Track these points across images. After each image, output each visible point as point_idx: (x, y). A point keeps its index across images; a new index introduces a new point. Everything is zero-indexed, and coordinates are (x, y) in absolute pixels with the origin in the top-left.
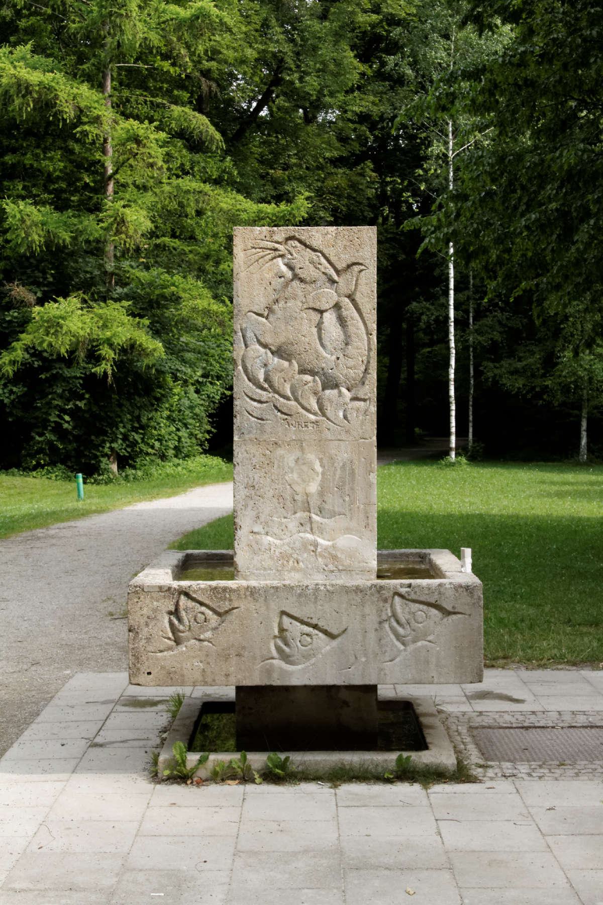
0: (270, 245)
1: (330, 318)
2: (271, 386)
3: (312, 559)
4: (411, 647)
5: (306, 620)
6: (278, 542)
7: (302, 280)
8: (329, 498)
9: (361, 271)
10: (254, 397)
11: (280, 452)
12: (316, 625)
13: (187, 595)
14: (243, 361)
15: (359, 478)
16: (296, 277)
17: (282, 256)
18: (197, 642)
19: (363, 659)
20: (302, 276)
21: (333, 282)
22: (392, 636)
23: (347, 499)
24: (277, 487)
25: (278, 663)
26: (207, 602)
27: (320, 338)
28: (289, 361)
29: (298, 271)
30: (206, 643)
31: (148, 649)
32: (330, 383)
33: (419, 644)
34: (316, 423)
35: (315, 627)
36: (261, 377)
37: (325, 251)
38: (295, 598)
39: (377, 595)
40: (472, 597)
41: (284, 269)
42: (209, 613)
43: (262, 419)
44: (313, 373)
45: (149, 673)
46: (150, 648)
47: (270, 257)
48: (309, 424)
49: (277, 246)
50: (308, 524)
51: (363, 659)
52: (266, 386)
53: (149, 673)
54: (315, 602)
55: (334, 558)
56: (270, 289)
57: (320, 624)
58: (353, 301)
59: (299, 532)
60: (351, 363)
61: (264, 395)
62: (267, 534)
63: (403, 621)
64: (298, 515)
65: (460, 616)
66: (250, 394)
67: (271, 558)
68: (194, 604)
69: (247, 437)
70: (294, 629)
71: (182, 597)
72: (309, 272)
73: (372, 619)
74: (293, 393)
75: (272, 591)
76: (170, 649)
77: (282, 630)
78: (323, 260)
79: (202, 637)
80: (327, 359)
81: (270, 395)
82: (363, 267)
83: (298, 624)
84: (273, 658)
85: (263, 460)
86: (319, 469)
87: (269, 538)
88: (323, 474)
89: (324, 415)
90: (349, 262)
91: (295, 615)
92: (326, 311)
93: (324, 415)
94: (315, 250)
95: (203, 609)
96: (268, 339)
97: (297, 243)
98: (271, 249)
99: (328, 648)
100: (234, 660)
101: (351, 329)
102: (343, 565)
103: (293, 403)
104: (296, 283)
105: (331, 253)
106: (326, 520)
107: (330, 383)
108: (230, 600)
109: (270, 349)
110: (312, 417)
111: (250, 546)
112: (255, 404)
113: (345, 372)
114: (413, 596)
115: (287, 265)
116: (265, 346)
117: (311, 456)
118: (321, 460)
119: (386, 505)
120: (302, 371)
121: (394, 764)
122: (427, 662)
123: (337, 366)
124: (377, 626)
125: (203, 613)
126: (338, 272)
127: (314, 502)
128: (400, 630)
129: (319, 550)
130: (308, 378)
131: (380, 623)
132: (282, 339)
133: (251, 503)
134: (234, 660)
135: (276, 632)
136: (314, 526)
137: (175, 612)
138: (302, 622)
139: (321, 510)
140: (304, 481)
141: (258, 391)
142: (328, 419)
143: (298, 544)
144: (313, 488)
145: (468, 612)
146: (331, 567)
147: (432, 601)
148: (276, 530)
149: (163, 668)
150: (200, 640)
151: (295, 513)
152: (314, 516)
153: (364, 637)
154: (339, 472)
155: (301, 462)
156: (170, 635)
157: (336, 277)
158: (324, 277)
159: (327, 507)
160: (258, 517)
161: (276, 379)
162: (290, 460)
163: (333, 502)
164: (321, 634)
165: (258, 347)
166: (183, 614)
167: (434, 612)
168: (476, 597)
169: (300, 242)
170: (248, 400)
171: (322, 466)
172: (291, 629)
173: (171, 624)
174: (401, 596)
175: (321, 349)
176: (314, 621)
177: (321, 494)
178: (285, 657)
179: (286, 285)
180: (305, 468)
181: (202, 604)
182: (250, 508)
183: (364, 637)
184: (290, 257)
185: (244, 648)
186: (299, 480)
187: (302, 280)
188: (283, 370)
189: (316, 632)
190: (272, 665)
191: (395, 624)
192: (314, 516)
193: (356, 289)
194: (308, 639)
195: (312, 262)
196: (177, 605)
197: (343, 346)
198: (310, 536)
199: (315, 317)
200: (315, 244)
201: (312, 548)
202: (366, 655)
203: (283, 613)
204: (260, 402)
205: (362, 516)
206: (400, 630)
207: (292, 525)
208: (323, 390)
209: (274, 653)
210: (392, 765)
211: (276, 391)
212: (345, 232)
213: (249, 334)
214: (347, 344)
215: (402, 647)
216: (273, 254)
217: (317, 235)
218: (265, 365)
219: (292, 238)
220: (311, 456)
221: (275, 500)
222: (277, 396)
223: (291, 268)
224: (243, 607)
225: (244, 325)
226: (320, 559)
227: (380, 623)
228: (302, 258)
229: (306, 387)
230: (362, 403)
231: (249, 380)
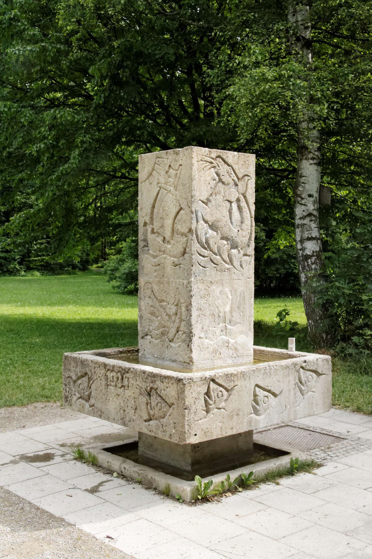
0: (210, 160)
1: (234, 206)
2: (209, 247)
3: (227, 351)
5: (266, 388)
6: (211, 342)
7: (223, 183)
8: (234, 314)
10: (201, 253)
11: (213, 287)
12: (270, 390)
13: (213, 380)
14: (196, 231)
16: (220, 180)
17: (214, 167)
18: (218, 410)
20: (223, 180)
23: (242, 314)
24: (212, 309)
26: (223, 384)
27: (231, 218)
28: (217, 231)
29: (222, 177)
30: (222, 410)
31: (195, 419)
32: (234, 246)
35: (269, 391)
37: (234, 166)
42: (223, 390)
43: (205, 267)
45: (196, 435)
46: (196, 418)
49: (212, 161)
50: (225, 330)
53: (196, 435)
55: (236, 349)
56: (209, 187)
58: (245, 197)
59: (221, 335)
61: (206, 252)
63: (304, 382)
65: (324, 376)
66: (199, 252)
67: (208, 352)
68: (217, 386)
69: (198, 278)
71: (211, 383)
72: (225, 179)
74: (218, 251)
78: (233, 172)
79: (220, 406)
80: (233, 231)
86: (230, 297)
87: (207, 341)
88: (232, 300)
89: (232, 264)
91: (262, 386)
93: (232, 264)
94: (229, 165)
95: (221, 389)
96: (208, 218)
97: (221, 160)
100: (235, 417)
101: (244, 214)
103: (218, 257)
104: (220, 184)
107: (234, 246)
108: (234, 381)
109: (209, 224)
110: (227, 266)
112: (201, 257)
114: (308, 368)
116: (206, 222)
118: (231, 291)
119: (260, 318)
120: (222, 238)
121: (289, 465)
122: (312, 403)
123: (238, 235)
125: (221, 391)
126: (238, 179)
129: (230, 345)
132: (214, 218)
133: (200, 319)
134: (235, 417)
136: (228, 331)
137: (208, 394)
138: (264, 390)
140: (224, 304)
142: (234, 267)
143: (221, 344)
144: (228, 309)
146: (235, 355)
148: (211, 336)
149: (202, 430)
150: (219, 409)
151: (219, 324)
153: (289, 394)
154: (238, 298)
155: (222, 293)
158: (233, 182)
159: (234, 319)
161: (211, 242)
172: (259, 395)
173: (206, 401)
175: (231, 225)
176: (269, 388)
177: (231, 312)
180: (224, 296)
181: (220, 385)
183: (289, 394)
185: (240, 410)
186: (222, 304)
189: (270, 394)
193: (246, 190)
195: (228, 172)
196: (209, 387)
197: (239, 224)
199: (228, 204)
200: (230, 161)
203: (257, 385)
204: (204, 256)
206: (303, 388)
212: (242, 156)
213: (199, 214)
216: (211, 165)
217: (231, 156)
221: (210, 317)
223: (218, 175)
224: (239, 384)
225: (197, 209)
226: (230, 351)
228: (223, 169)
230: (248, 257)
231: (198, 242)
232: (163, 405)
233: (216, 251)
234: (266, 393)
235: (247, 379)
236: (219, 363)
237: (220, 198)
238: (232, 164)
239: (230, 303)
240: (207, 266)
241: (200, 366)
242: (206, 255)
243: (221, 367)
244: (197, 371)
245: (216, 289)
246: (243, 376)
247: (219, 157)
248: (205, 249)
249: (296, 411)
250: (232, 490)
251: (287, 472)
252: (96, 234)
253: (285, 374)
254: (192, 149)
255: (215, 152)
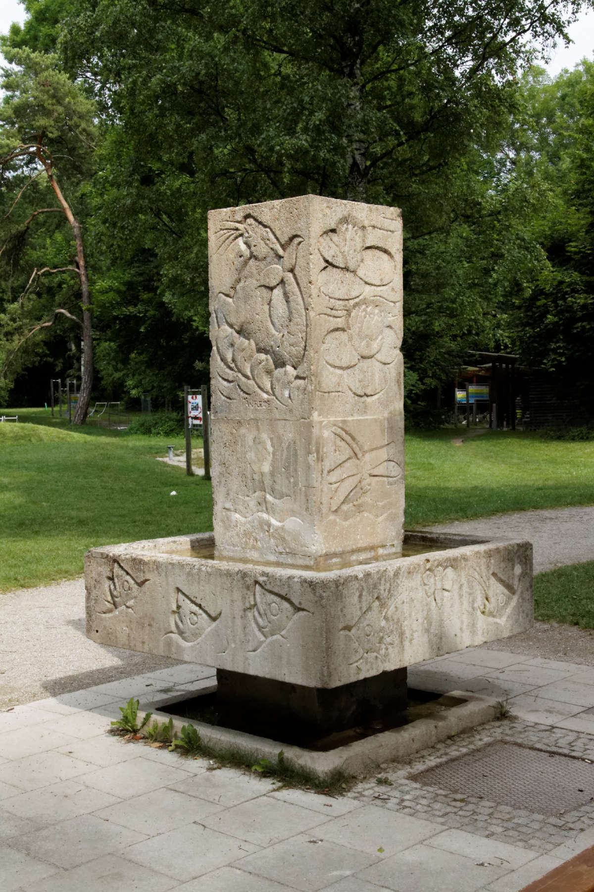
4: (270, 639)
7: (256, 258)
9: (300, 243)
11: (243, 431)
15: (300, 459)
19: (233, 646)
21: (280, 257)
22: (254, 625)
25: (175, 637)
33: (275, 637)
34: (267, 402)
35: (200, 606)
36: (229, 360)
38: (185, 577)
39: (242, 582)
40: (314, 594)
41: (243, 247)
43: (230, 399)
44: (266, 352)
47: (232, 237)
48: (263, 404)
49: (238, 225)
50: (262, 503)
51: (233, 646)
52: (233, 365)
54: (199, 583)
55: (283, 539)
57: (203, 605)
60: (293, 339)
61: (230, 374)
62: (235, 511)
63: (262, 611)
64: (257, 494)
65: (305, 613)
70: (188, 606)
72: (262, 250)
73: (239, 606)
75: (170, 567)
76: (110, 611)
77: (179, 607)
78: (271, 236)
81: (235, 374)
82: (300, 239)
83: (189, 602)
84: (172, 632)
85: (230, 438)
86: (271, 449)
87: (237, 516)
88: (274, 454)
90: (290, 236)
92: (275, 287)
94: (265, 226)
95: (128, 578)
96: (232, 320)
98: (233, 229)
99: (209, 629)
102: (289, 548)
103: (251, 382)
105: (275, 226)
106: (277, 501)
110: (265, 396)
111: (223, 521)
113: (288, 349)
114: (268, 587)
115: (246, 243)
116: (231, 326)
117: (265, 436)
118: (271, 439)
120: (260, 350)
122: (280, 658)
123: (282, 343)
124: (242, 613)
126: (282, 246)
127: (268, 482)
128: (260, 620)
130: (263, 356)
131: (245, 610)
133: (223, 480)
135: (174, 608)
138: (193, 602)
139: (273, 491)
141: (228, 370)
144: (266, 468)
145: (312, 610)
146: (281, 549)
147: (283, 593)
148: (241, 508)
152: (268, 496)
153: (233, 622)
156: (109, 598)
157: (281, 252)
158: (272, 252)
160: (228, 494)
162: (250, 438)
163: (282, 484)
164: (204, 615)
165: (227, 327)
166: (116, 580)
167: (286, 605)
168: (317, 594)
169: (256, 220)
170: (220, 379)
171: (273, 446)
174: (260, 585)
176: (198, 601)
177: (272, 474)
178: (181, 633)
179: (246, 263)
180: (260, 447)
181: (128, 573)
182: (223, 483)
183: (233, 622)
184: (247, 235)
187: (256, 258)
188: (244, 350)
189: (201, 612)
190: (171, 638)
191: (256, 614)
192: (268, 496)
194: (195, 618)
198: (265, 516)
201: (266, 528)
202: (235, 642)
205: (303, 497)
206: (260, 620)
207: (252, 504)
208: (276, 368)
209: (173, 628)
210: (275, 761)
211: (240, 371)
213: (220, 315)
214: (290, 321)
215: (263, 638)
217: (266, 210)
218: (232, 345)
219: (248, 216)
220: (265, 436)
222: (240, 375)
227: (245, 610)
228: (256, 233)
229: (261, 366)
231: (222, 360)
232: (365, 624)
233: (249, 374)
234: (196, 609)
235: (163, 574)
236: (254, 555)
237: (253, 283)
238: (269, 223)
239: (270, 458)
240: (233, 396)
241: (225, 553)
242: (230, 379)
243: (257, 563)
244: (222, 558)
245: (248, 434)
246: (157, 569)
247: (248, 216)
248: (231, 369)
249: (247, 659)
250: (268, 772)
251: (291, 777)
252: (152, 355)
253: (225, 586)
254: (307, 198)
255: (241, 210)
